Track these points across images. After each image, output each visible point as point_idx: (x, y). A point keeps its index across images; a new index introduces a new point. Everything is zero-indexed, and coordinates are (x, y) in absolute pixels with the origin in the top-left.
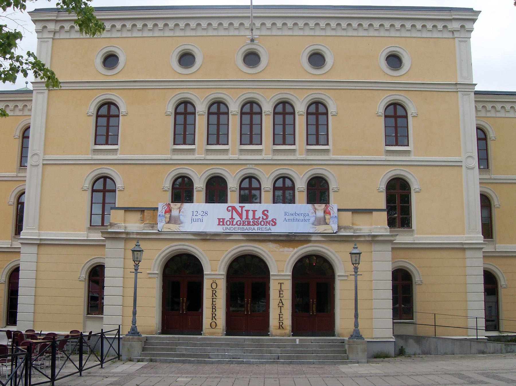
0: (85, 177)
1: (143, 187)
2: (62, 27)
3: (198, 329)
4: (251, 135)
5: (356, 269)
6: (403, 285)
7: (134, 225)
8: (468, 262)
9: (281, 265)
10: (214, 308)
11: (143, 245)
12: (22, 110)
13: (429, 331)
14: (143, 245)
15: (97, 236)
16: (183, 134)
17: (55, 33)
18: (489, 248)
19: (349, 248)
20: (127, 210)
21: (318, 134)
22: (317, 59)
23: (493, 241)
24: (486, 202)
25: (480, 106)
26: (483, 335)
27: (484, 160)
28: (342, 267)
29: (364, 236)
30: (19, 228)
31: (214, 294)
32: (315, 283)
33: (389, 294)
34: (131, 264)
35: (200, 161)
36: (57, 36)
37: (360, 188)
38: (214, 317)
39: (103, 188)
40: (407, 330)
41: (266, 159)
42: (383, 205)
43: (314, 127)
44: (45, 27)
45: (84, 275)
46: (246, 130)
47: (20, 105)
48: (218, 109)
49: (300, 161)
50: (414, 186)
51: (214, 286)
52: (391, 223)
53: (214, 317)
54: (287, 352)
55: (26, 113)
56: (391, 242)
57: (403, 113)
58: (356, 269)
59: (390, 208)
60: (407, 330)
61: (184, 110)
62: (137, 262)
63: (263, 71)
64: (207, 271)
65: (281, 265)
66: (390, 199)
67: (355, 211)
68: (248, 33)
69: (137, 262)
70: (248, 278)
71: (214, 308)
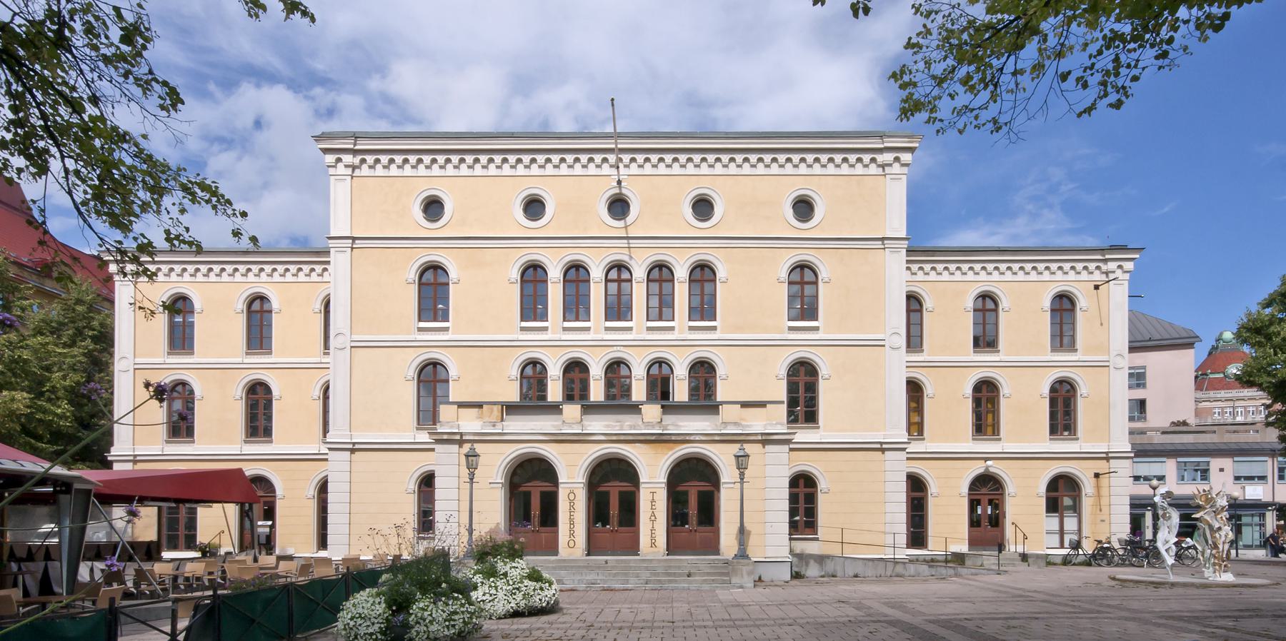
0: (409, 363)
1: (484, 377)
2: (363, 161)
3: (633, 548)
4: (618, 309)
5: (742, 475)
6: (803, 492)
7: (470, 423)
8: (888, 465)
9: (653, 471)
10: (572, 523)
11: (479, 448)
12: (270, 275)
13: (835, 550)
14: (479, 448)
15: (424, 437)
16: (533, 307)
17: (354, 168)
18: (916, 447)
19: (735, 448)
20: (461, 405)
21: (704, 309)
22: (703, 207)
23: (271, 442)
24: (915, 389)
25: (915, 267)
26: (905, 553)
27: (914, 341)
28: (728, 473)
29: (756, 434)
30: (325, 430)
31: (572, 506)
32: (695, 491)
33: (785, 505)
34: (465, 472)
35: (555, 341)
36: (357, 172)
37: (750, 377)
38: (572, 534)
39: (431, 377)
40: (811, 548)
41: (638, 341)
42: (783, 395)
43: (657, 298)
44: (339, 160)
45: (413, 485)
46: (655, 302)
47: (319, 268)
48: (660, 272)
49: (680, 342)
50: (823, 371)
51: (572, 497)
52: (793, 418)
53: (572, 534)
54: (655, 575)
55: (326, 277)
56: (788, 442)
57: (586, 278)
58: (742, 475)
59: (793, 403)
60: (811, 548)
61: (533, 274)
62: (472, 468)
63: (548, 224)
64: (562, 478)
65: (653, 471)
66: (792, 388)
67: (745, 405)
68: (614, 171)
69: (472, 468)
70: (612, 486)
71: (572, 523)
